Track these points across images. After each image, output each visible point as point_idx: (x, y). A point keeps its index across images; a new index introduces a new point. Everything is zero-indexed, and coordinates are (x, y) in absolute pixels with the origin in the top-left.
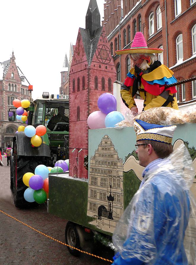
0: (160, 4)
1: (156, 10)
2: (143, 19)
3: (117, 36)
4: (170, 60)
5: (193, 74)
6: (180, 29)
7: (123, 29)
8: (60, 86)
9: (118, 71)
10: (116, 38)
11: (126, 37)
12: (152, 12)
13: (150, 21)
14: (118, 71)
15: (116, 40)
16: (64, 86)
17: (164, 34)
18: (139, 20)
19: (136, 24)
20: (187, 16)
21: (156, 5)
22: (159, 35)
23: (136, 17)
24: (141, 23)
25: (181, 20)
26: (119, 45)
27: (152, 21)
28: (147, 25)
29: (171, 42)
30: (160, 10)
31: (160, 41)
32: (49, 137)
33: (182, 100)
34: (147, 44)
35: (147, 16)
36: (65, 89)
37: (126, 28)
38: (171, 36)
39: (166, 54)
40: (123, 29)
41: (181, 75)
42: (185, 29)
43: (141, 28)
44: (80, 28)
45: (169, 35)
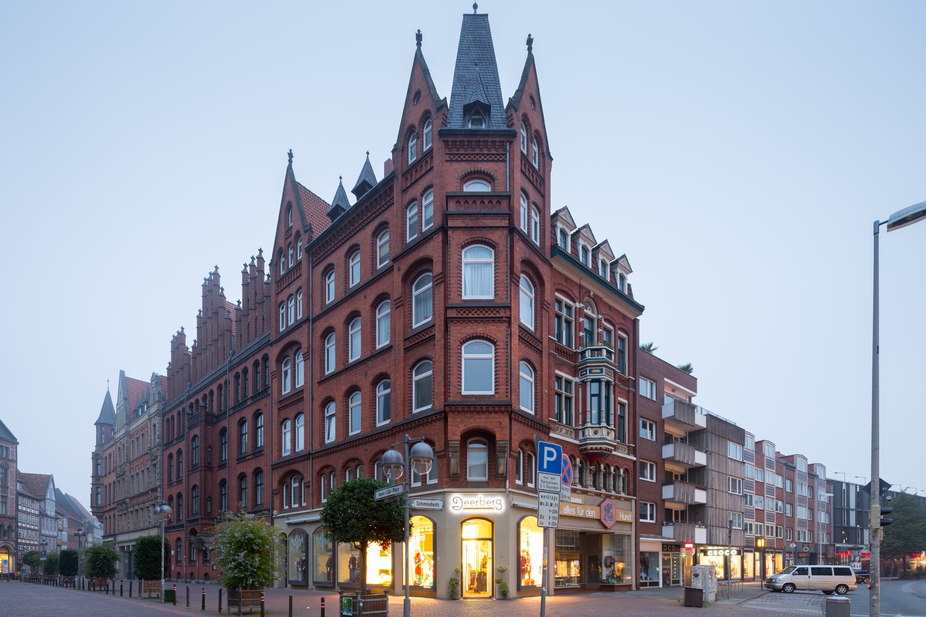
0: (302, 347)
1: (295, 354)
2: (272, 364)
3: (222, 381)
4: (314, 438)
5: (349, 464)
6: (331, 394)
7: (234, 372)
8: (94, 450)
9: (224, 442)
10: (237, 374)
11: (223, 397)
12: (288, 356)
13: (284, 369)
14: (224, 442)
15: (220, 387)
16: (104, 451)
17: (307, 396)
18: (257, 370)
19: (260, 369)
20: (343, 376)
21: (295, 348)
22: (297, 397)
23: (259, 357)
24: (267, 370)
25: (334, 381)
26: (225, 398)
27: (287, 371)
28: (278, 375)
29: (275, 428)
30: (301, 358)
31: (299, 407)
32: (841, 483)
33: (291, 506)
34: (404, 345)
35: (281, 358)
36: (106, 457)
37: (240, 372)
38: (318, 403)
39: (308, 430)
40: (234, 372)
41: (330, 463)
42: (339, 395)
43: (267, 378)
44: (464, 15)
45: (314, 401)
